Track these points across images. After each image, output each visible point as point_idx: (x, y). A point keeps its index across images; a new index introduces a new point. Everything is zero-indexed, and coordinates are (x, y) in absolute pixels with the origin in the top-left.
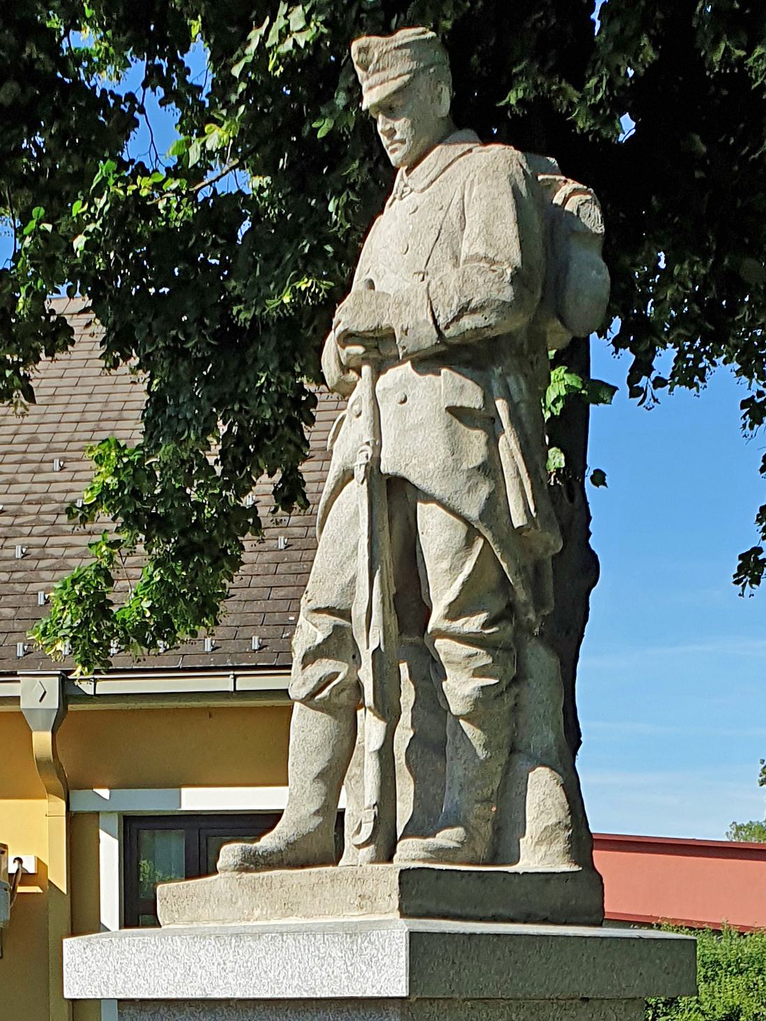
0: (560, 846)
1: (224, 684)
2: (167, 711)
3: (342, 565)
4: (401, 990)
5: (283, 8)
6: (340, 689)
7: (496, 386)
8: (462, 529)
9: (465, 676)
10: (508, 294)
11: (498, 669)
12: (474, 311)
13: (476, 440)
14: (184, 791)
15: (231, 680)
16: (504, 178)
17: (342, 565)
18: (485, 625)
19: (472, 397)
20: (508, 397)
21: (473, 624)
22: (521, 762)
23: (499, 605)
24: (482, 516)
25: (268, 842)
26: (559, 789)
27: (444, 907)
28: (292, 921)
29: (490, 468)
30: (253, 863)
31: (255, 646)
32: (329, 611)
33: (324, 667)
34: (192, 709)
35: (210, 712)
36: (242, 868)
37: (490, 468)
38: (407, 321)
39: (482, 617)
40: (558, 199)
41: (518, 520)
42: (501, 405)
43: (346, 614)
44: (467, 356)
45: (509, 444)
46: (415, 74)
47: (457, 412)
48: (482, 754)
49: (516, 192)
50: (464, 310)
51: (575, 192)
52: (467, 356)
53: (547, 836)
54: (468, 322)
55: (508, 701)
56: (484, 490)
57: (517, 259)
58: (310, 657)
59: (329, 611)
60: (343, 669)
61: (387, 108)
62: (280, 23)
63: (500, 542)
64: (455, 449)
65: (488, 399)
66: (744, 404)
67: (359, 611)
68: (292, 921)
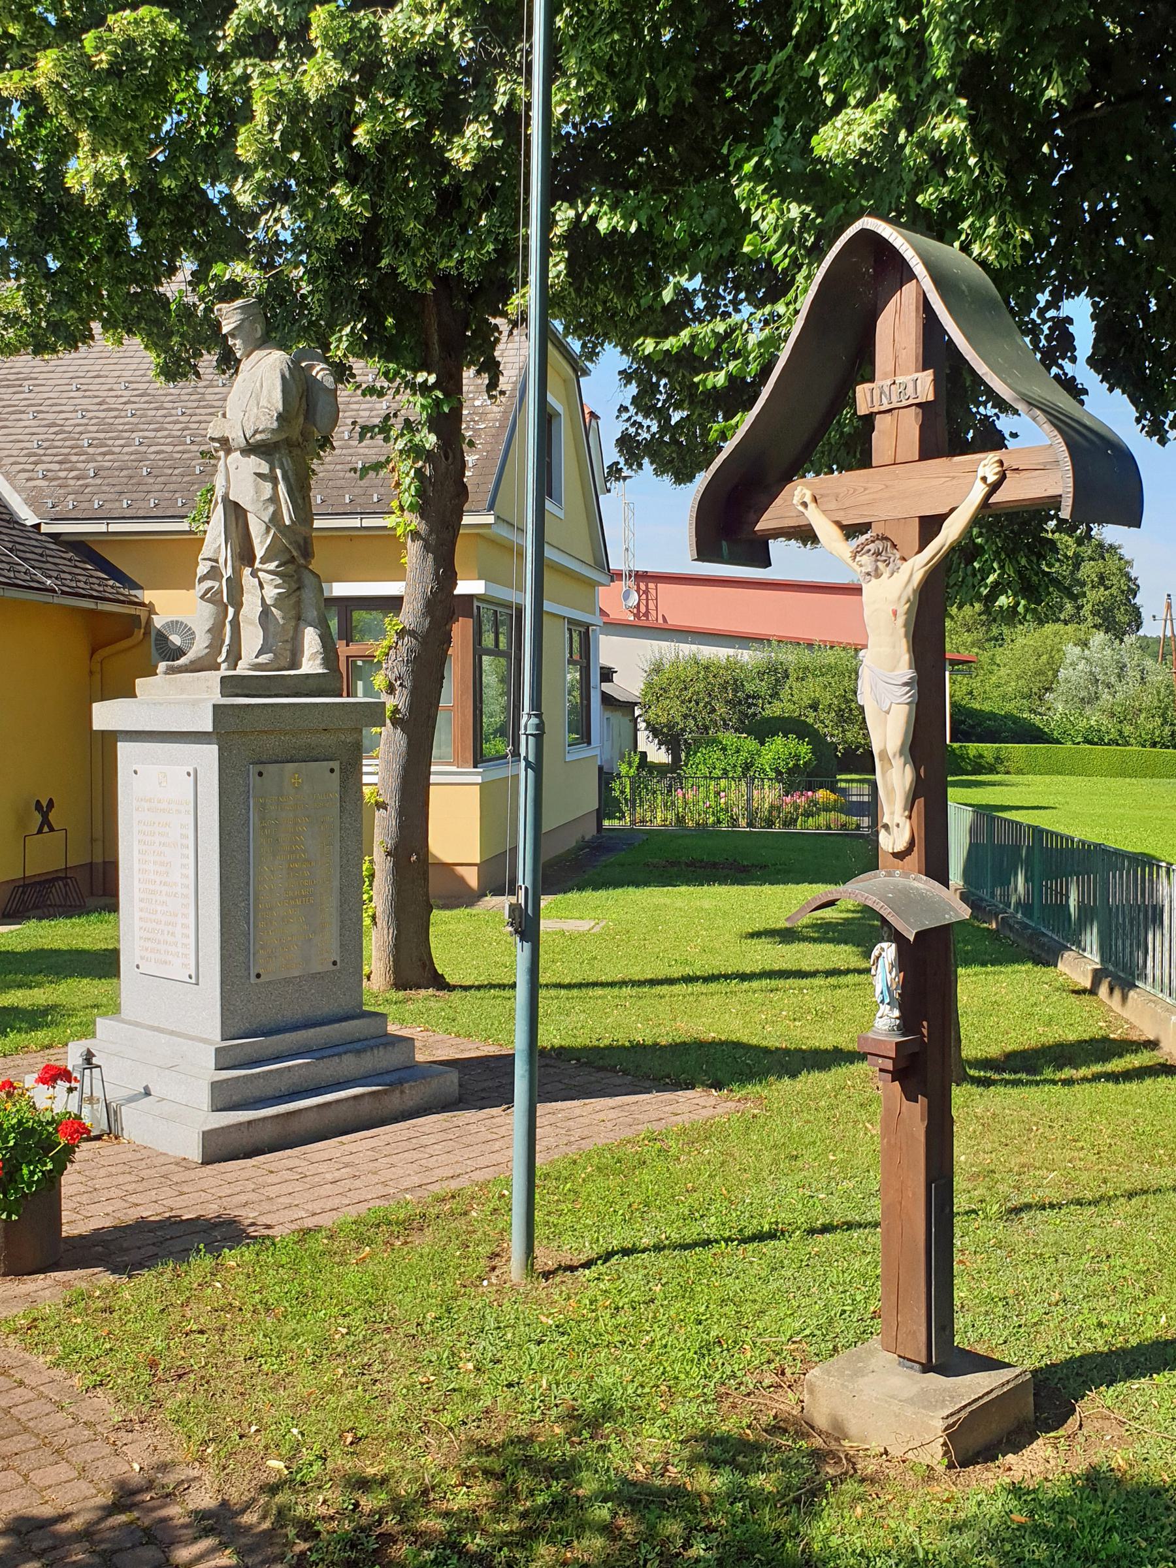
0: (319, 661)
1: (355, 523)
2: (325, 537)
3: (215, 539)
4: (211, 730)
5: (278, 206)
6: (216, 593)
7: (276, 463)
8: (264, 526)
9: (272, 588)
10: (275, 425)
11: (286, 585)
12: (260, 432)
13: (268, 486)
14: (334, 584)
15: (359, 520)
16: (278, 371)
17: (215, 539)
18: (277, 567)
19: (265, 468)
20: (282, 468)
21: (272, 566)
22: (302, 624)
23: (287, 557)
24: (270, 521)
25: (183, 661)
26: (317, 638)
27: (247, 692)
28: (184, 696)
29: (274, 499)
30: (171, 671)
31: (375, 500)
32: (209, 559)
33: (208, 584)
34: (340, 536)
35: (351, 538)
36: (166, 673)
37: (274, 499)
38: (234, 436)
39: (276, 563)
40: (314, 373)
41: (288, 522)
42: (279, 472)
43: (216, 561)
44: (263, 449)
45: (282, 488)
46: (243, 320)
47: (259, 475)
48: (281, 622)
49: (283, 377)
50: (256, 432)
51: (322, 369)
52: (263, 449)
53: (313, 657)
54: (258, 437)
55: (293, 599)
56: (271, 509)
57: (281, 409)
58: (203, 579)
59: (209, 559)
60: (216, 585)
61: (232, 334)
62: (276, 214)
63: (280, 532)
64: (258, 491)
65: (272, 469)
66: (620, 373)
67: (222, 560)
68: (184, 696)
